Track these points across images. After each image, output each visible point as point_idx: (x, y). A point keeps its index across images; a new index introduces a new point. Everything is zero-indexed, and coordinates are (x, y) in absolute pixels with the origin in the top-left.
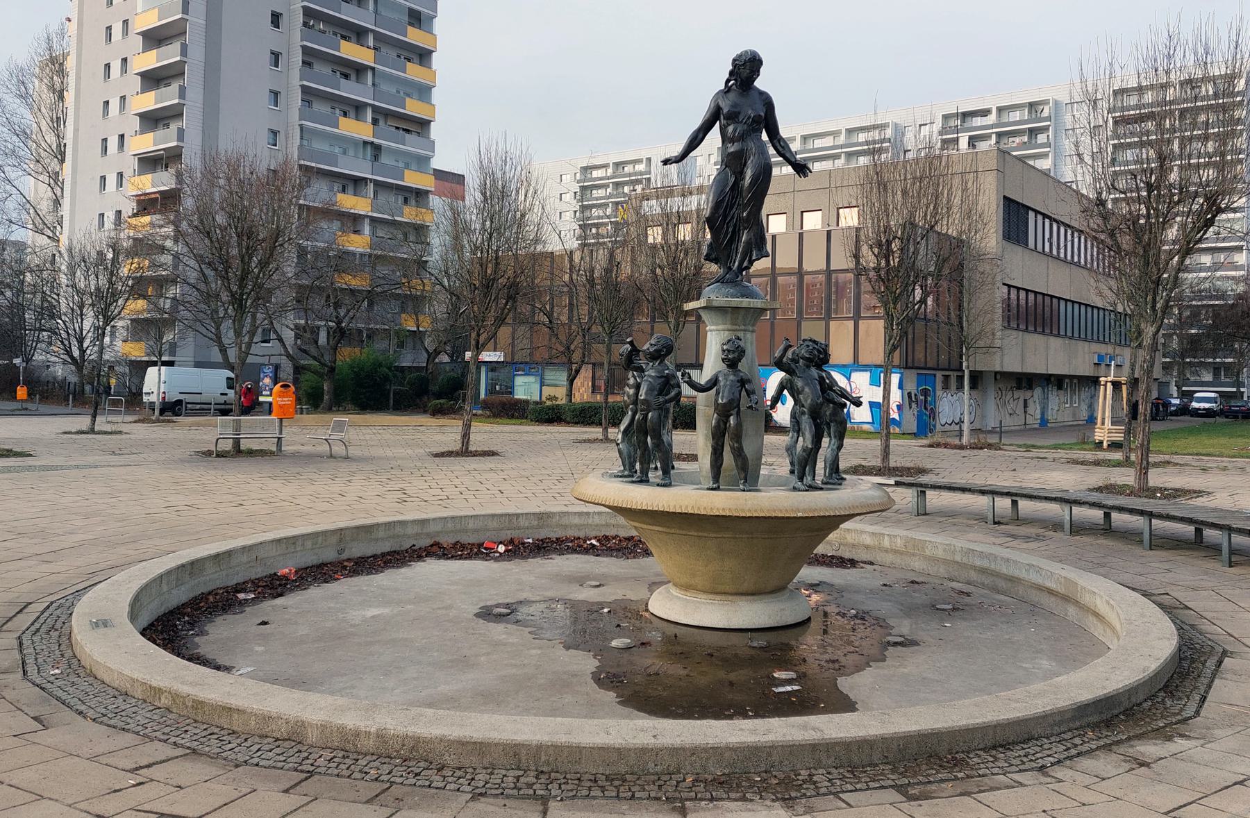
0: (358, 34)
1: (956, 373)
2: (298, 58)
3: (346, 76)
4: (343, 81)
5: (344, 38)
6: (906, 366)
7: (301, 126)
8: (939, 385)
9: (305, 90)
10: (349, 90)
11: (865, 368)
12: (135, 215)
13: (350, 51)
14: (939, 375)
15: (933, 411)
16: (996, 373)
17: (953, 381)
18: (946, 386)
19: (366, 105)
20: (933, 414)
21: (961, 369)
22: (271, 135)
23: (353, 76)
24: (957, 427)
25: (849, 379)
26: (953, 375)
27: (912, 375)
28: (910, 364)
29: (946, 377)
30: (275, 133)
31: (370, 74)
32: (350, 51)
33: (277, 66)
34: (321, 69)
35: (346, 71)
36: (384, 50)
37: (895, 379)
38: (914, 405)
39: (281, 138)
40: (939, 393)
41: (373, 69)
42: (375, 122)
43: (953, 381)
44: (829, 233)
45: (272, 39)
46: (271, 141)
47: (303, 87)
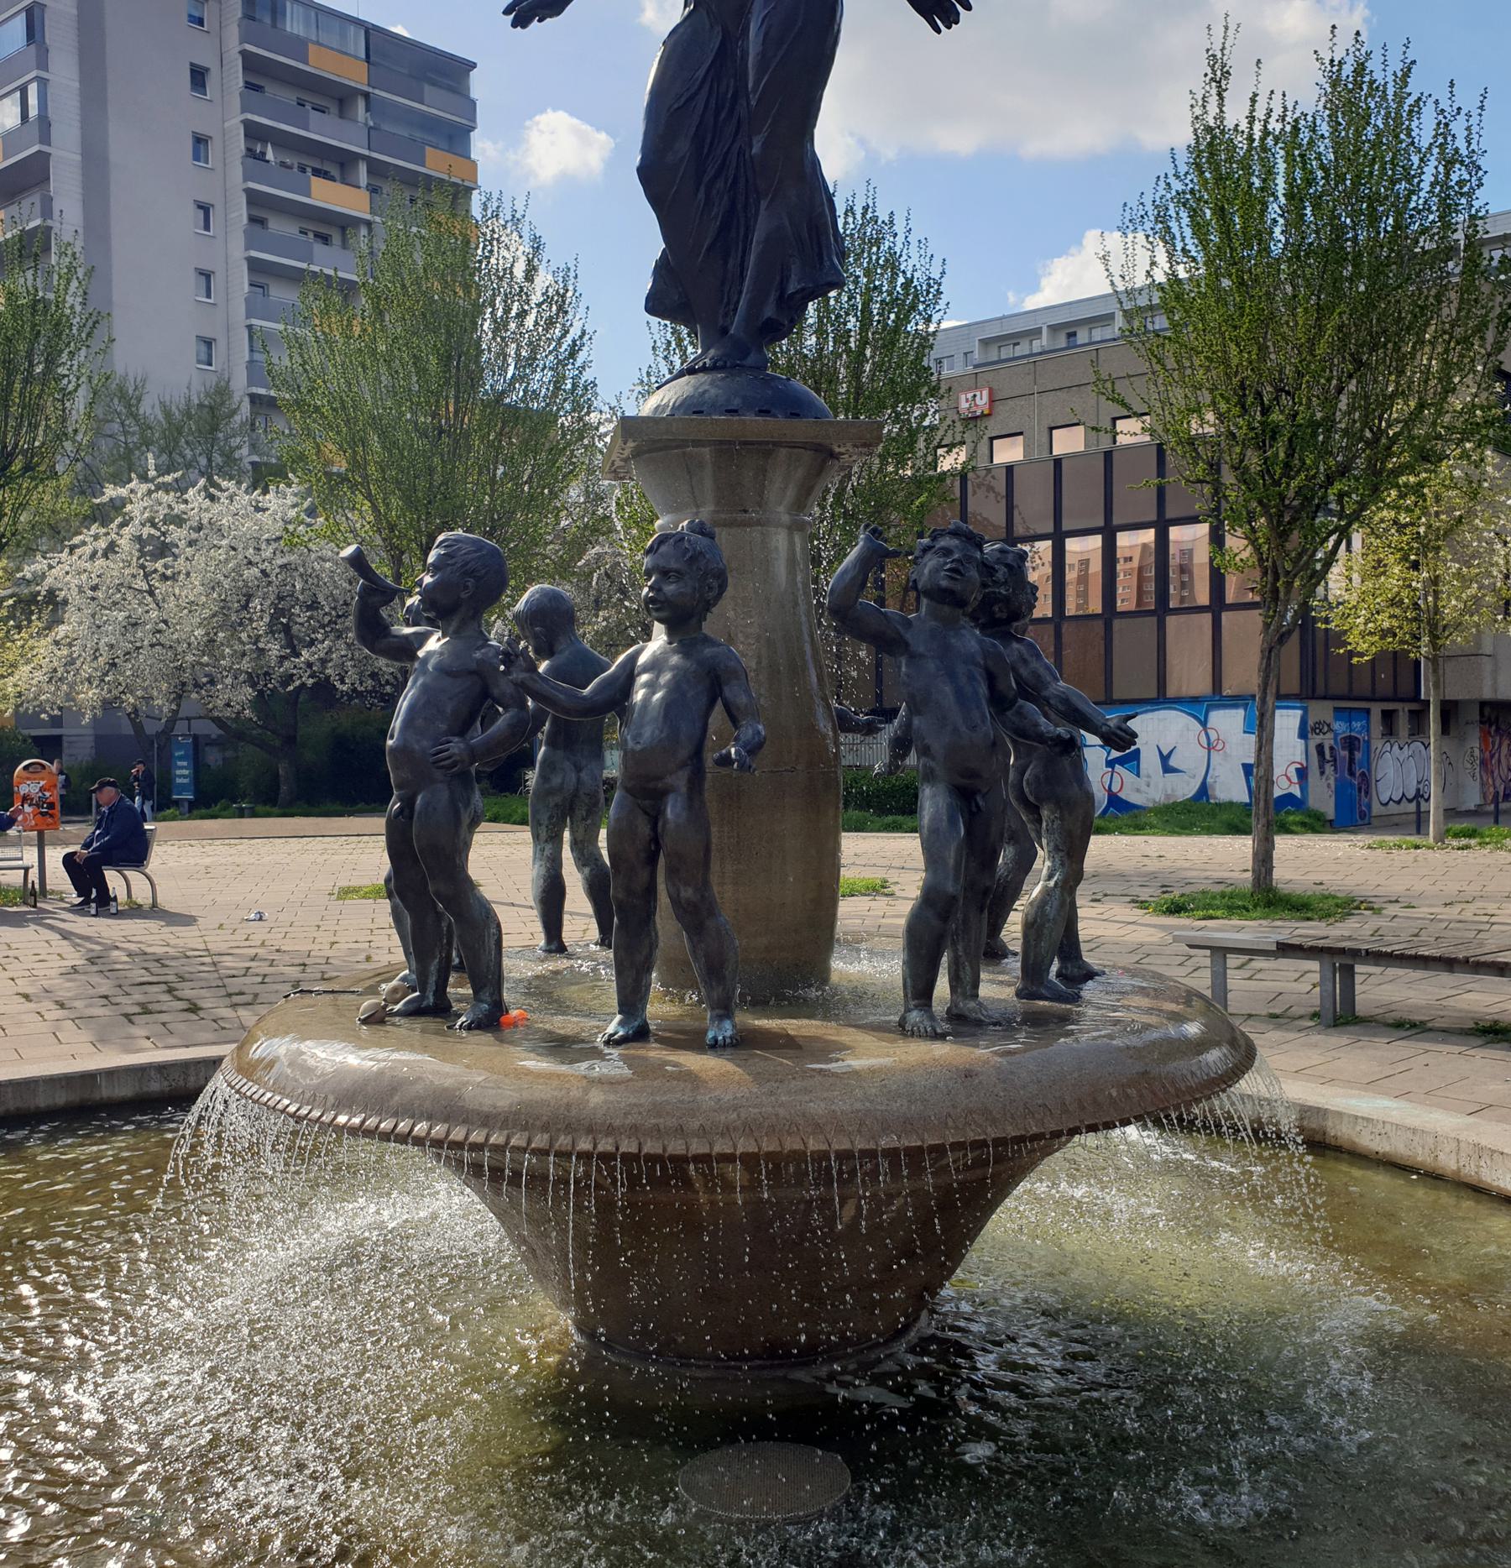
0: (338, 164)
1: (1408, 707)
2: (237, 78)
3: (325, 239)
4: (314, 115)
5: (317, 172)
6: (1307, 693)
7: (250, 327)
8: (1377, 726)
9: (255, 266)
10: (322, 130)
11: (1235, 701)
12: (215, 1063)
13: (326, 195)
14: (1376, 709)
15: (1365, 778)
16: (1483, 704)
17: (1403, 724)
18: (1390, 730)
19: (357, 157)
20: (1366, 783)
21: (1416, 697)
22: (203, 348)
23: (336, 238)
24: (1412, 807)
25: (1204, 724)
26: (1403, 710)
27: (1322, 711)
28: (1320, 690)
29: (1388, 716)
30: (209, 343)
31: (364, 231)
32: (326, 195)
33: (207, 227)
34: (280, 226)
35: (323, 230)
36: (387, 188)
37: (1287, 722)
38: (1329, 769)
39: (219, 352)
40: (1377, 744)
41: (366, 95)
42: (373, 190)
43: (1403, 724)
44: (1160, 451)
45: (196, 114)
46: (204, 357)
47: (250, 193)
